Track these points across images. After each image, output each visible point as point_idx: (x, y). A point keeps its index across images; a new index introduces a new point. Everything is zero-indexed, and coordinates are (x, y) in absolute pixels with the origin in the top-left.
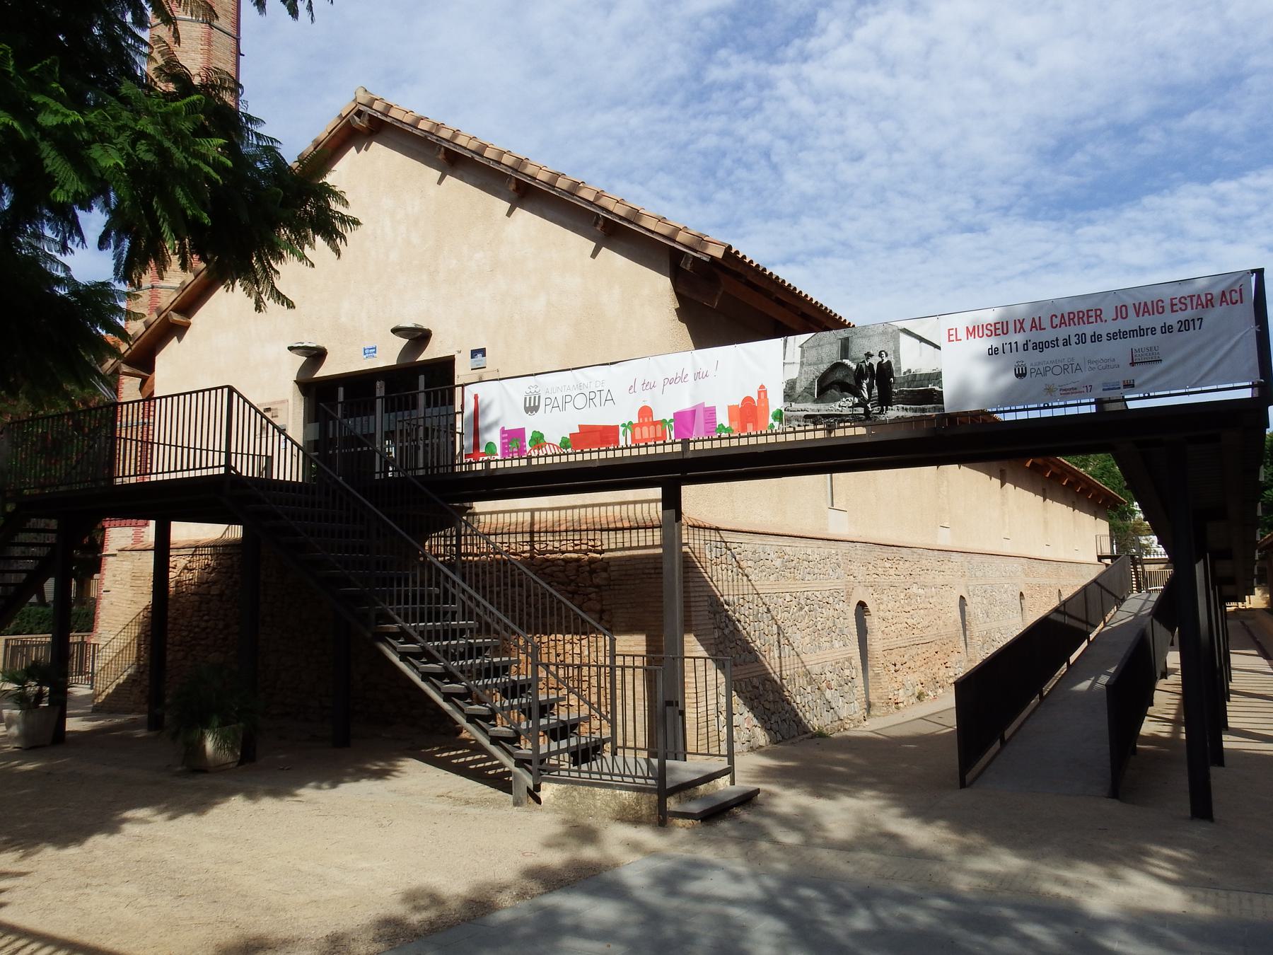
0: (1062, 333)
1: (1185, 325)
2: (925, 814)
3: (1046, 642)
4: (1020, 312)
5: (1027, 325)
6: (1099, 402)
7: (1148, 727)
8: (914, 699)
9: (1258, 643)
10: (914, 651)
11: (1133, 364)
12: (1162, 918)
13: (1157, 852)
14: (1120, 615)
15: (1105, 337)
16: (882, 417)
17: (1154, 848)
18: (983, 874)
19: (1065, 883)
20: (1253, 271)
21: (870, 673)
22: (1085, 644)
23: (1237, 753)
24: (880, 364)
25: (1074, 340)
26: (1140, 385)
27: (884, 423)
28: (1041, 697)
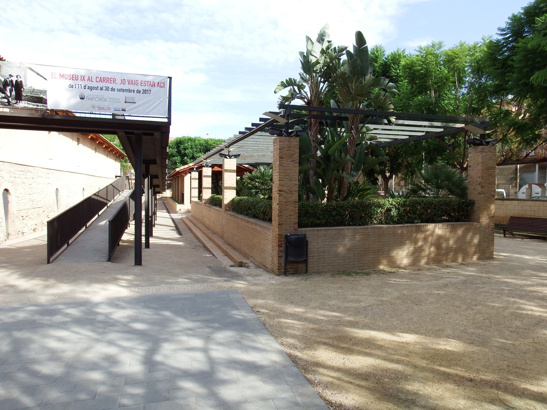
0: (100, 85)
1: (145, 92)
2: (27, 275)
3: (89, 207)
4: (82, 73)
5: (86, 78)
6: (113, 115)
7: (125, 237)
8: (32, 231)
9: (167, 208)
10: (33, 210)
11: (126, 102)
12: (119, 299)
13: (249, 337)
14: (120, 197)
15: (116, 90)
16: (16, 105)
17: (120, 277)
18: (53, 295)
19: (86, 293)
20: (169, 77)
21: (10, 220)
22: (106, 207)
23: (156, 245)
24: (16, 81)
25: (104, 88)
26: (128, 111)
27: (17, 108)
28: (86, 227)
